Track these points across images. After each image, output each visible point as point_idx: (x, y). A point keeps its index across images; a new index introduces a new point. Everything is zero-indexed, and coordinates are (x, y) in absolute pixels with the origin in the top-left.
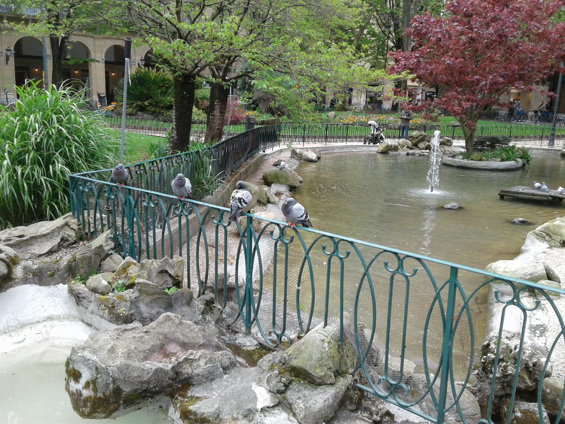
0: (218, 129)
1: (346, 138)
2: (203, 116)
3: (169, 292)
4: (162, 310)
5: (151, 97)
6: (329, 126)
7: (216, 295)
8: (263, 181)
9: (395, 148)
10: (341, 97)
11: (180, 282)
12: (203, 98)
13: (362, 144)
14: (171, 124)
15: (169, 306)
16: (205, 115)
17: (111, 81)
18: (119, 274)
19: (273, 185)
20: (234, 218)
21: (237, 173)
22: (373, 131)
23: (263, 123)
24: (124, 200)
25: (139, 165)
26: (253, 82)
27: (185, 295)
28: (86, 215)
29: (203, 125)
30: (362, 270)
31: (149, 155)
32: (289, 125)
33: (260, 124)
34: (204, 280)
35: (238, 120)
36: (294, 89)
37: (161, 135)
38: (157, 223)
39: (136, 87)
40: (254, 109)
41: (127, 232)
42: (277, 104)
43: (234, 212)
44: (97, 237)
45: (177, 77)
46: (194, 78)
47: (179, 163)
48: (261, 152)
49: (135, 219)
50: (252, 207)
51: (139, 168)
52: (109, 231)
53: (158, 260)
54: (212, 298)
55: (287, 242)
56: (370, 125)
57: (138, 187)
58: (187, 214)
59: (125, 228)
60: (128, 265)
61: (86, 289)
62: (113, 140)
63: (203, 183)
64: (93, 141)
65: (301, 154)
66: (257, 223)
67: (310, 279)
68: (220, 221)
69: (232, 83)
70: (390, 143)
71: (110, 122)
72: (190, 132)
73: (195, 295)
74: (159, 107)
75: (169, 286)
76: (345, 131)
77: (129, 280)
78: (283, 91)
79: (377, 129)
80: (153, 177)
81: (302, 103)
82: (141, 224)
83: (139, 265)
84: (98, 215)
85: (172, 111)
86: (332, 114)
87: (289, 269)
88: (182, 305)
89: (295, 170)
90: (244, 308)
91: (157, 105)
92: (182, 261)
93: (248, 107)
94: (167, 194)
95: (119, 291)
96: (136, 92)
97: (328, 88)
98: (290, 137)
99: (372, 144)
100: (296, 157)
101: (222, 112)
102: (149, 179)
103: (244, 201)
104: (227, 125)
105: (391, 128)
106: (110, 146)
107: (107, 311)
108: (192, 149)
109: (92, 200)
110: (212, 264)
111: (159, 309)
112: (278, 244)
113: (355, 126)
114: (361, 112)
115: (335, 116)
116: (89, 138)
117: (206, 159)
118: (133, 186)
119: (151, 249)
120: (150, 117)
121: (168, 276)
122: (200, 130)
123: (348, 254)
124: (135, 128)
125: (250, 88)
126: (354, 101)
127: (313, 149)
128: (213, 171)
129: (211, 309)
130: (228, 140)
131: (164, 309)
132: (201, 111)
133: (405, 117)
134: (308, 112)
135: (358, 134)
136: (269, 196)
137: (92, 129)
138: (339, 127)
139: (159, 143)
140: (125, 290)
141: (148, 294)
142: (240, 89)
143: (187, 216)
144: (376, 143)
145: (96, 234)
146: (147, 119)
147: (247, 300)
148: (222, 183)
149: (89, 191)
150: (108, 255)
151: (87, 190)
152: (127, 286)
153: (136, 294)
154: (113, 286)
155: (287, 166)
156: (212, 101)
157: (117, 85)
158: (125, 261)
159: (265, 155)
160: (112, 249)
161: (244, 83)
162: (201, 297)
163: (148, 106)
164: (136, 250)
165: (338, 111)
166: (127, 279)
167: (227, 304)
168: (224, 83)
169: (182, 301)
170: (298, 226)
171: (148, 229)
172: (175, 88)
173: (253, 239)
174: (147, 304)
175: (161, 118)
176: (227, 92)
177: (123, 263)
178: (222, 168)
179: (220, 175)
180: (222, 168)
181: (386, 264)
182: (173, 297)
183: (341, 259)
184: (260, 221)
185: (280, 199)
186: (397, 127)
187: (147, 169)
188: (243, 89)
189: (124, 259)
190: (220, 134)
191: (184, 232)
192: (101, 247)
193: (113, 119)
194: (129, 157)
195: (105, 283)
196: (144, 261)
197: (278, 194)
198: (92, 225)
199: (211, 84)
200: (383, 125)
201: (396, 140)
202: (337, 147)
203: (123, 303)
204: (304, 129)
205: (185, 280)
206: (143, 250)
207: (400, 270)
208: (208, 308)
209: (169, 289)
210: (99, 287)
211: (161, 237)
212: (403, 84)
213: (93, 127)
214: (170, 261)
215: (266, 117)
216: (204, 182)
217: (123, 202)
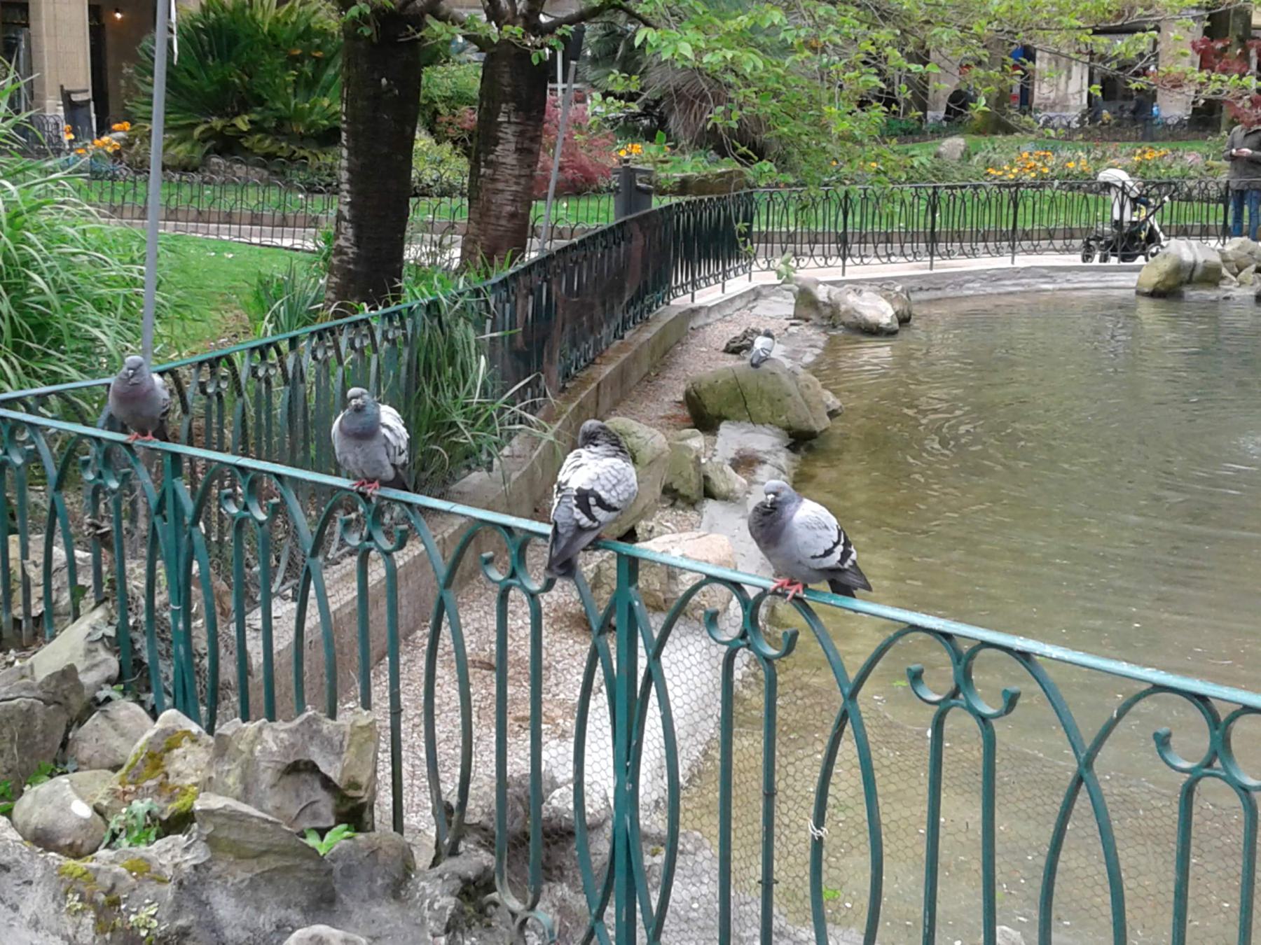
0: (513, 216)
1: (1012, 238)
2: (456, 168)
3: (322, 847)
4: (295, 915)
5: (260, 101)
6: (943, 193)
7: (500, 859)
8: (685, 413)
9: (1210, 276)
10: (988, 81)
11: (363, 806)
12: (454, 100)
13: (1076, 259)
14: (335, 199)
15: (322, 899)
16: (463, 164)
17: (110, 40)
18: (136, 777)
19: (725, 429)
20: (564, 566)
21: (584, 384)
22: (1118, 211)
23: (684, 186)
24: (154, 498)
25: (214, 363)
26: (642, 34)
27: (382, 856)
28: (14, 551)
29: (456, 202)
30: (1070, 766)
31: (251, 320)
32: (785, 192)
33: (673, 193)
34: (454, 801)
35: (589, 180)
36: (799, 57)
37: (298, 243)
38: (279, 579)
39: (202, 64)
40: (650, 136)
41: (167, 614)
42: (736, 115)
43: (563, 543)
44: (53, 637)
45: (354, 23)
46: (419, 23)
47: (361, 351)
48: (681, 301)
49: (195, 567)
50: (643, 515)
51: (213, 374)
52: (99, 613)
53: (280, 725)
54: (486, 869)
55: (771, 652)
56: (1107, 186)
57: (208, 447)
58: (388, 546)
59: (159, 600)
60: (171, 741)
61: (12, 835)
62: (116, 269)
63: (453, 424)
64: (41, 274)
65: (834, 307)
66: (663, 575)
67: (863, 799)
68: (513, 575)
69: (563, 38)
70: (1188, 257)
71: (107, 197)
72: (403, 231)
73: (423, 858)
74: (291, 137)
75: (321, 824)
76: (1007, 211)
77: (172, 799)
78: (755, 68)
79: (1135, 201)
80: (264, 402)
81: (831, 110)
82: (221, 585)
83: (211, 740)
84: (59, 552)
85: (336, 149)
86: (954, 144)
87: (780, 761)
88: (372, 895)
89: (814, 369)
90: (610, 910)
91: (280, 129)
92: (371, 727)
93: (628, 129)
94: (320, 471)
95: (138, 841)
96: (205, 82)
97: (938, 49)
98: (791, 238)
99: (1114, 261)
100: (814, 317)
101: (528, 151)
102: (251, 412)
103: (601, 503)
104: (545, 198)
105: (1189, 198)
106: (104, 291)
107: (89, 919)
108: (414, 295)
109: (38, 497)
110: (485, 735)
111: (283, 913)
112: (738, 662)
113: (1048, 192)
114: (1070, 133)
115: (967, 155)
116: (26, 264)
117: (464, 332)
118: (190, 444)
119: (257, 679)
120: (255, 174)
121: (317, 785)
122: (445, 218)
123: (1012, 701)
124: (201, 217)
125: (632, 60)
126: (1042, 92)
127: (883, 286)
128: (492, 377)
129: (482, 911)
130: (550, 257)
131: (305, 911)
132: (448, 146)
133: (1247, 151)
134: (861, 144)
135: (1060, 220)
136: (709, 469)
137: (38, 229)
138: (983, 196)
139: (291, 273)
140: (158, 837)
141: (242, 854)
142: (594, 60)
143: (388, 554)
144: (1134, 257)
145: (51, 625)
146: (247, 183)
147: (620, 880)
148: (529, 424)
149: (26, 463)
150: (96, 704)
151: (18, 460)
152: (163, 823)
153: (199, 854)
154: (114, 825)
155: (778, 352)
156: (488, 111)
157: (134, 58)
158: (159, 725)
159: (694, 312)
160: (110, 681)
161: (613, 36)
162: (442, 866)
163: (249, 133)
164: (200, 686)
165: (978, 132)
166: (166, 795)
167: (545, 895)
168: (531, 40)
169: (372, 879)
170: (814, 592)
171: (244, 602)
172: (348, 64)
173: (640, 642)
174: (239, 894)
175: (298, 177)
176: (546, 72)
177: (150, 733)
178: (528, 364)
179: (521, 394)
180: (528, 364)
181: (1163, 742)
182: (337, 866)
183: (984, 719)
184: (671, 572)
185: (751, 483)
186: (1213, 193)
187: (244, 373)
188: (605, 58)
189: (155, 718)
190: (520, 234)
191: (379, 614)
192: (68, 674)
193: (119, 186)
194: (178, 331)
195: (82, 810)
196: (229, 726)
197: (745, 463)
198: (37, 592)
199: (482, 43)
200: (1158, 186)
201: (1213, 242)
202: (976, 275)
203: (150, 889)
204: (846, 205)
205: (385, 798)
206: (227, 686)
207: (1217, 764)
208: (470, 909)
209: (322, 833)
210: (61, 824)
211: (290, 636)
212: (1235, 24)
213: (43, 219)
214: (327, 725)
215: (693, 165)
216: (460, 421)
217: (153, 504)
